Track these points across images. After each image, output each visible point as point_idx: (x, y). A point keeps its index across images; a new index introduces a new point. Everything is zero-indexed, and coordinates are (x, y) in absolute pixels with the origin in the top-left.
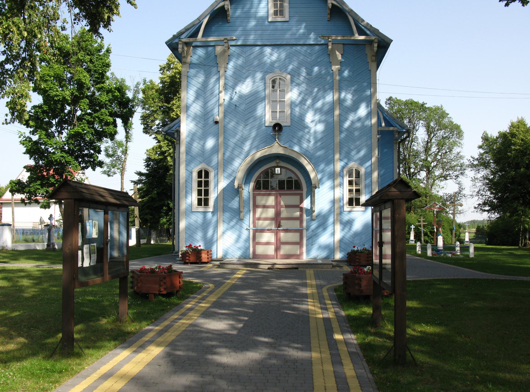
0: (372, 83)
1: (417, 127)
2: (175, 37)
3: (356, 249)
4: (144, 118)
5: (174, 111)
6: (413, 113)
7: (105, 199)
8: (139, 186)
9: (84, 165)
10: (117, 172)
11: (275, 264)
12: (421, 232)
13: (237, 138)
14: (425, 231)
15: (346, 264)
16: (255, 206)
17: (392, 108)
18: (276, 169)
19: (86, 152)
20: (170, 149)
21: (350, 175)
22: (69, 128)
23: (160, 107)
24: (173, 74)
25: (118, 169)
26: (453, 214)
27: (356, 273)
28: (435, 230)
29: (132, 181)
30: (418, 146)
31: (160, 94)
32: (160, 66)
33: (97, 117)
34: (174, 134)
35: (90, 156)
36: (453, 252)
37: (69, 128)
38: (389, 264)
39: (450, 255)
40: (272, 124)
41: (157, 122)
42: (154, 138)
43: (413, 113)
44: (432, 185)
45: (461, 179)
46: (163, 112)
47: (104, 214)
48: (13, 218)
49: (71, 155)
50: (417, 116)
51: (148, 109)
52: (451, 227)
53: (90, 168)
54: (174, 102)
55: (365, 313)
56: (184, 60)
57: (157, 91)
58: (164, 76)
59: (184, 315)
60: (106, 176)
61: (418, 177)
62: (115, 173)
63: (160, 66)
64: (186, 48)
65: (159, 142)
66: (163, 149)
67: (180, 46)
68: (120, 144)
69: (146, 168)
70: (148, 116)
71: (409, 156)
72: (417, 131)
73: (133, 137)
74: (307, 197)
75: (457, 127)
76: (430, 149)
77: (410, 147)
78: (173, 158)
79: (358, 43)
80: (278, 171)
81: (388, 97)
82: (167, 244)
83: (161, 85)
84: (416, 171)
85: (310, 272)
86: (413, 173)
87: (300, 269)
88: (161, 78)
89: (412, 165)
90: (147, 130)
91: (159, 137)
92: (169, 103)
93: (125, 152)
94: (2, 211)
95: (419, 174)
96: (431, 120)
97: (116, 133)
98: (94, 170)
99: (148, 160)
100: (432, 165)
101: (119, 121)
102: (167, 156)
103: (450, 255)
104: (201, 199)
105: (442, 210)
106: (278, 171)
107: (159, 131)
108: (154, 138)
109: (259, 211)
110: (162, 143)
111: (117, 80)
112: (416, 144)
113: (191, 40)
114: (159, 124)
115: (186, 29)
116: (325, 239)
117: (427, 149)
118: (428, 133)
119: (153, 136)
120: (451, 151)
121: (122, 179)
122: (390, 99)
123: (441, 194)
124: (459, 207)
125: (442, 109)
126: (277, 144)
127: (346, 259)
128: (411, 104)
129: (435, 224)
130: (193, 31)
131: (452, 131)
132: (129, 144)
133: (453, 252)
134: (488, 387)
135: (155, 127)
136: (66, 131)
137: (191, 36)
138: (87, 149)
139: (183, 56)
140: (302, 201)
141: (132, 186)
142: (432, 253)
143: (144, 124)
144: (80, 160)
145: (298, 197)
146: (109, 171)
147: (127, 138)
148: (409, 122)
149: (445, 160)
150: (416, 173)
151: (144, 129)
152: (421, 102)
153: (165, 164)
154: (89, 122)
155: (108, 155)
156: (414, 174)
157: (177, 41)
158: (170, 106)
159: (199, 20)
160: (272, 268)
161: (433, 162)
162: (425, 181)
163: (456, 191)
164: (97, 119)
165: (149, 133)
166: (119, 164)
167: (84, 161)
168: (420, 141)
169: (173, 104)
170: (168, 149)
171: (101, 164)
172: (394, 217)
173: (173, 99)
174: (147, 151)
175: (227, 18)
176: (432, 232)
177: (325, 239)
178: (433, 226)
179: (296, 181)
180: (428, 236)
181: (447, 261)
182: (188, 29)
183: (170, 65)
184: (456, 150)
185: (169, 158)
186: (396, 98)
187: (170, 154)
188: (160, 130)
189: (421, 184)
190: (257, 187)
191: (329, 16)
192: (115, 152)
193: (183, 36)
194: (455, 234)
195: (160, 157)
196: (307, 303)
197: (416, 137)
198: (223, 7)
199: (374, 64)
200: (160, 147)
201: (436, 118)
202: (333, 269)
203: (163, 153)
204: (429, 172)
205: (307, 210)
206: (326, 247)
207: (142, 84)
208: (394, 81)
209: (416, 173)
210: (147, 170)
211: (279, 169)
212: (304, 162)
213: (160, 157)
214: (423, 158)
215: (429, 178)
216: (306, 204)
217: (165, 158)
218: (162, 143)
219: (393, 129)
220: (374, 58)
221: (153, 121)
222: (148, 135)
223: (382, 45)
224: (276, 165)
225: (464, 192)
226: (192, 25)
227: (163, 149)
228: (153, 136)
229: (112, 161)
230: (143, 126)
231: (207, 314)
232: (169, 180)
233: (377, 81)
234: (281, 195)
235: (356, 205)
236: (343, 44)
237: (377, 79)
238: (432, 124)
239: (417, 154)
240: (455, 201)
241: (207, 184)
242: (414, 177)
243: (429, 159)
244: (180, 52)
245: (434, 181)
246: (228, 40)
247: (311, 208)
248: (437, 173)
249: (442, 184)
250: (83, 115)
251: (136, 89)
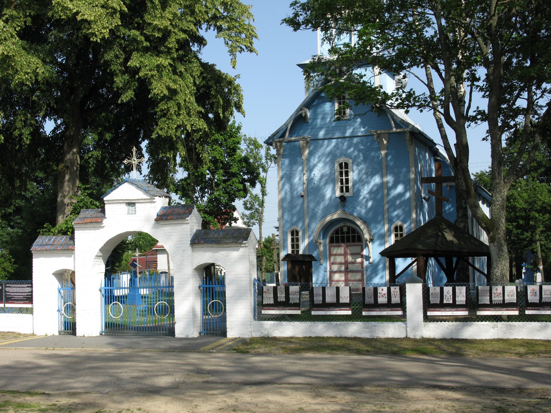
13: (402, 174)
16: (330, 255)
48: (169, 266)
93: (262, 204)
94: (157, 258)
109: (332, 258)
113: (281, 139)
115: (277, 132)
121: (260, 229)
134: (13, 185)
137: (280, 137)
140: (362, 250)
145: (359, 248)
146: (249, 222)
157: (271, 141)
159: (286, 125)
193: (275, 138)
234: (347, 246)
241: (298, 240)
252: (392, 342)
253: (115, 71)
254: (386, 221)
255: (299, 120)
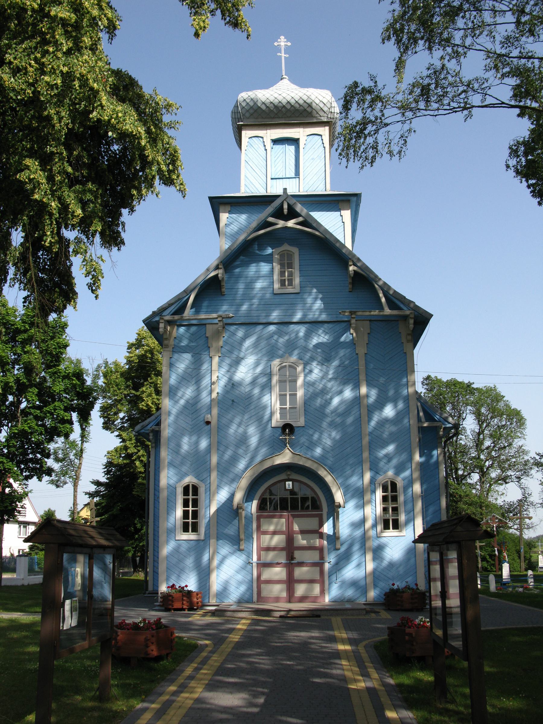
0: (406, 366)
1: (464, 415)
2: (154, 314)
3: (395, 587)
4: (104, 410)
5: (143, 400)
6: (458, 396)
7: (95, 541)
8: (96, 499)
9: (27, 473)
10: (68, 481)
11: (290, 610)
12: (477, 557)
14: (483, 554)
15: (384, 607)
17: (430, 390)
18: (287, 483)
19: (31, 456)
20: (139, 451)
21: (385, 489)
22: (10, 424)
23: (126, 396)
24: (143, 352)
25: (70, 477)
26: (521, 530)
27: (405, 626)
28: (497, 553)
29: (86, 493)
30: (466, 439)
31: (127, 379)
32: (128, 343)
33: (49, 412)
34: (148, 434)
35: (35, 461)
36: (525, 585)
37: (10, 424)
38: (439, 609)
39: (521, 590)
40: (281, 424)
41: (121, 415)
42: (117, 436)
43: (458, 396)
44: (488, 491)
45: (525, 481)
46: (130, 402)
47: (89, 559)
49: (12, 460)
50: (463, 400)
51: (110, 398)
52: (518, 548)
53: (35, 477)
54: (144, 389)
55: (419, 681)
56: (166, 342)
57: (122, 374)
58: (131, 355)
59: (183, 688)
60: (54, 487)
61: (469, 481)
62: (65, 483)
63: (128, 343)
64: (169, 328)
65: (124, 441)
66: (129, 451)
67: (162, 325)
68: (73, 444)
69: (106, 476)
70: (110, 407)
71: (455, 454)
72: (464, 419)
73: (91, 435)
74: (328, 519)
75: (517, 413)
76: (482, 444)
77: (456, 441)
78: (146, 465)
79: (387, 320)
80: (289, 485)
81: (425, 375)
82: (132, 578)
83: (127, 367)
84: (466, 473)
85: (337, 620)
86: (462, 475)
87: (322, 617)
88: (127, 358)
89: (460, 466)
90: (108, 426)
91: (124, 435)
92: (137, 390)
93: (80, 454)
95: (470, 477)
96: (482, 405)
97: (72, 431)
98: (40, 480)
99: (109, 465)
100: (487, 464)
101: (75, 416)
102: (135, 460)
103: (521, 590)
104: (189, 522)
105: (502, 525)
106: (289, 485)
107: (123, 426)
108: (117, 436)
110: (128, 443)
111: (72, 362)
112: (463, 437)
113: (176, 317)
114: (124, 417)
116: (350, 572)
117: (479, 443)
118: (479, 423)
119: (116, 433)
120: (510, 445)
121: (75, 491)
122: (428, 378)
123: (500, 502)
124: (527, 520)
125: (495, 390)
126: (287, 451)
127: (382, 601)
128: (454, 385)
129: (495, 545)
130: (178, 306)
131: (510, 419)
132: (85, 445)
133: (525, 585)
135: (119, 421)
136: (6, 428)
137: (175, 313)
138: (31, 453)
139: (165, 337)
140: (321, 525)
141: (86, 499)
142: (496, 587)
143: (104, 417)
144: (23, 466)
145: (316, 521)
146: (58, 481)
147: (83, 437)
148: (453, 409)
149: (502, 457)
150: (466, 476)
151: (103, 424)
152: (466, 382)
153: (132, 470)
154: (37, 418)
155: (57, 460)
156: (464, 477)
157: (157, 319)
158: (138, 393)
159: (187, 292)
160: (287, 616)
161: (487, 460)
162: (478, 487)
163: (520, 498)
164: (48, 415)
165: (110, 429)
166: (71, 471)
167: (27, 469)
168: (469, 432)
169: (143, 392)
170: (136, 451)
171: (49, 472)
172: (462, 562)
173: (143, 385)
174: (108, 453)
175: (221, 289)
176: (492, 556)
177: (350, 572)
178: (494, 547)
179: (313, 498)
180: (488, 562)
181: (516, 597)
182: (172, 304)
183: (141, 341)
184: (517, 443)
185: (137, 463)
186: (436, 377)
187: (139, 457)
188: (126, 425)
189: (474, 491)
190: (261, 507)
191: (350, 286)
192: (66, 455)
193: (165, 313)
194: (525, 557)
195: (125, 462)
196: (337, 666)
197: (464, 429)
198: (216, 276)
199: (411, 344)
200: (126, 448)
201: (488, 402)
202: (367, 617)
203: (129, 456)
204: (483, 474)
205: (329, 536)
206: (354, 584)
207: (103, 368)
208: (433, 359)
209: (466, 476)
210: (107, 479)
211: (291, 483)
212: (322, 473)
213: (125, 462)
214: (473, 455)
215: (483, 482)
216: (327, 528)
217: (133, 462)
218: (128, 443)
219: (434, 420)
220: (409, 338)
221: (116, 414)
222: (108, 433)
223: (420, 320)
224: (286, 478)
225: (531, 499)
226: (178, 298)
227: (129, 451)
228: (116, 433)
229: (61, 467)
230: (102, 420)
231: (213, 686)
232: (136, 492)
233: (415, 366)
234: (294, 516)
235: (393, 529)
236: (370, 321)
237: (415, 363)
238: (483, 410)
239: (464, 451)
240: (520, 512)
242: (463, 482)
243: (482, 457)
244: (161, 333)
245: (491, 485)
246: (223, 318)
247: (334, 533)
248: (494, 474)
249: (500, 488)
250: (29, 408)
251: (95, 373)
252: (260, 121)
253: (432, 403)
254: (366, 466)
255: (210, 289)
